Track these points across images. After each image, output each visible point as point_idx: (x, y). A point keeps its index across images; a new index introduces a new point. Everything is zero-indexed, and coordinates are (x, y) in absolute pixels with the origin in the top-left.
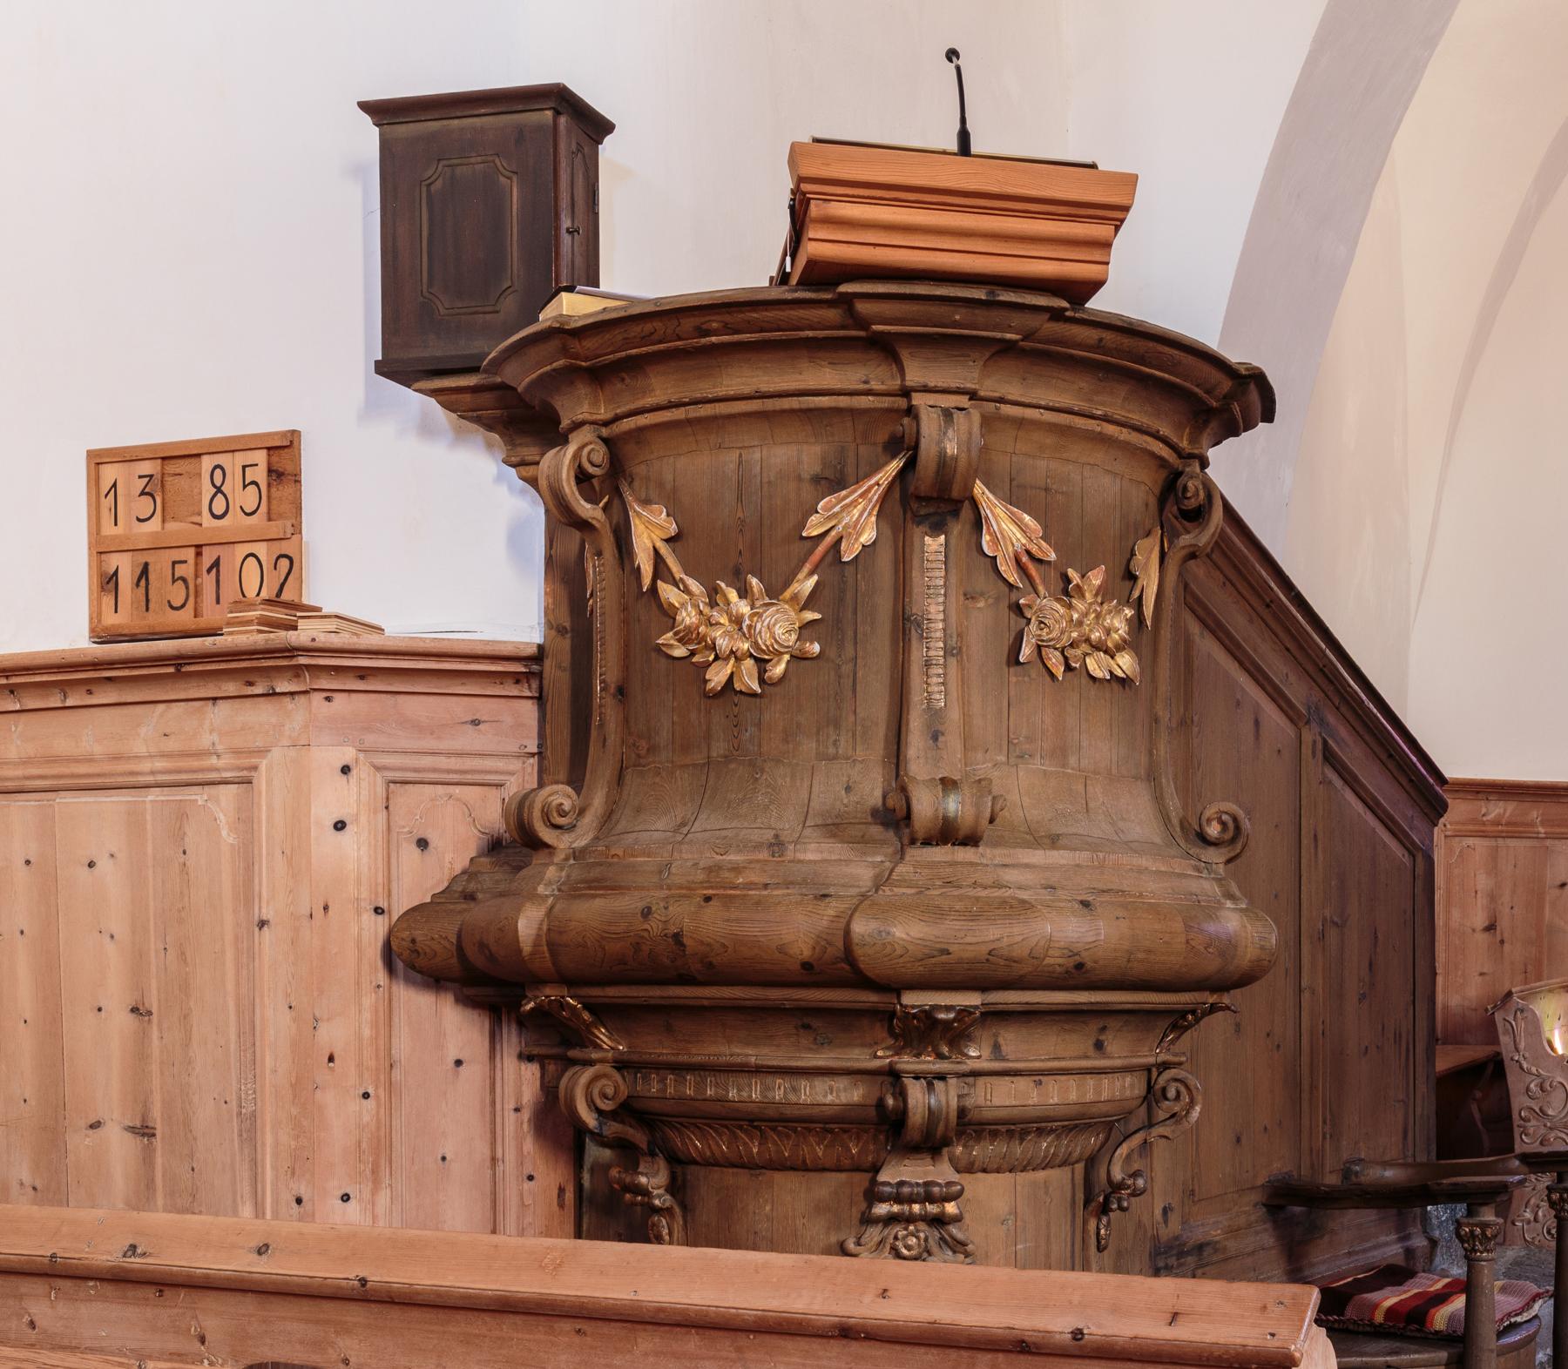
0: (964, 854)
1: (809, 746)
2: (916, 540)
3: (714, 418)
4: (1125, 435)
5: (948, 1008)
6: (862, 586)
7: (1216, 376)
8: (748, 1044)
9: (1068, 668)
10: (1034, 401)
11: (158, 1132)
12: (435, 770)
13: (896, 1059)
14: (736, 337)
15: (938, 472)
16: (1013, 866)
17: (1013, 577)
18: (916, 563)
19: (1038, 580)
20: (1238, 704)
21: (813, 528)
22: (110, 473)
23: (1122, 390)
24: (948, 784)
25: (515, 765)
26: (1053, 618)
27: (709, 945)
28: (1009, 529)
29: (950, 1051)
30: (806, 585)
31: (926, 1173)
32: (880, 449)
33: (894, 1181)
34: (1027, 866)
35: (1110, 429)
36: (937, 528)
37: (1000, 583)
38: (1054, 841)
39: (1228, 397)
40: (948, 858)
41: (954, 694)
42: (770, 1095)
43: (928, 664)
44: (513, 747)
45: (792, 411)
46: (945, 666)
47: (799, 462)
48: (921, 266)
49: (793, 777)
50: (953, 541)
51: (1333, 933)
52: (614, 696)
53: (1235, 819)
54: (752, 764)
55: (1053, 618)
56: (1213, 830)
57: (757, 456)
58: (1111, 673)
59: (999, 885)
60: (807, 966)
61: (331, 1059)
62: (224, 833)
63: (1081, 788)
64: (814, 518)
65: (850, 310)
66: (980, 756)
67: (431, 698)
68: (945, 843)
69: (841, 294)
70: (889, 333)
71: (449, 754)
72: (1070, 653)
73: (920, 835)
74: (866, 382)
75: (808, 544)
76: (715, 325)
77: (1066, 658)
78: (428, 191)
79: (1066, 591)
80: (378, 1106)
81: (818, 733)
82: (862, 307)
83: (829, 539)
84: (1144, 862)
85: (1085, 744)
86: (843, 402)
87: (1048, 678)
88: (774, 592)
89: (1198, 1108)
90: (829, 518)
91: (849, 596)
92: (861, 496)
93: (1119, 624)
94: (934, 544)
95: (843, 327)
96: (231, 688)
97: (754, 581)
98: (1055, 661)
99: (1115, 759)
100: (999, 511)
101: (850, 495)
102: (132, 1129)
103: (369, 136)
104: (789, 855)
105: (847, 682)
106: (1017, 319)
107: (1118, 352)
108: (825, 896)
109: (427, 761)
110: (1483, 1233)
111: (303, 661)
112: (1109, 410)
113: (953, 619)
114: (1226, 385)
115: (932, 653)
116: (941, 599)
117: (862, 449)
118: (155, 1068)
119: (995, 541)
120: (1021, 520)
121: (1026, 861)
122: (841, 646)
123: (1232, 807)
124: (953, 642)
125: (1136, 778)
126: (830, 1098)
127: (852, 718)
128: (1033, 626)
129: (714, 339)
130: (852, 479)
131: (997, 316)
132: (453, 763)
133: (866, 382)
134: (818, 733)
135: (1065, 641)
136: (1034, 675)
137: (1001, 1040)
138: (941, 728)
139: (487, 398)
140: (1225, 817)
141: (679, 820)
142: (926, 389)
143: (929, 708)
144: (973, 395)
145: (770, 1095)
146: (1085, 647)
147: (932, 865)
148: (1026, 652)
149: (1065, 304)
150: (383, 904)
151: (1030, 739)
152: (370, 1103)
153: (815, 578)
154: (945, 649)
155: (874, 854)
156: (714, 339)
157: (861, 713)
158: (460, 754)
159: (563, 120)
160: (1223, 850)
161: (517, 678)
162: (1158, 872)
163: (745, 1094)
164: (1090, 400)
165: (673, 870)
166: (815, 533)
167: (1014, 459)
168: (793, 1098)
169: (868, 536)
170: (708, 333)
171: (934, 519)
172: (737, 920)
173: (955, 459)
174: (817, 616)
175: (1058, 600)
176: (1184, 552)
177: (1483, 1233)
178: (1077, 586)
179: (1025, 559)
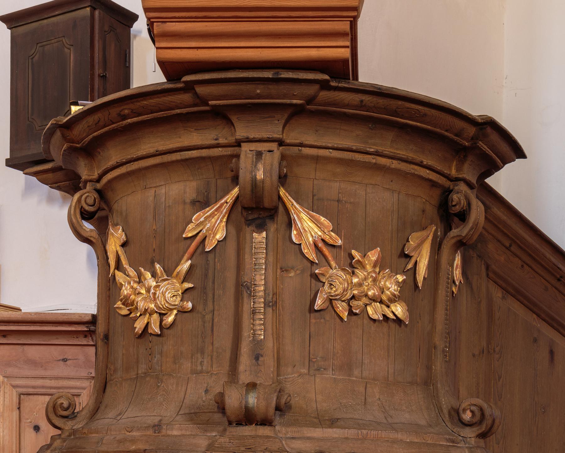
2: (248, 236)
3: (140, 170)
4: (395, 164)
6: (218, 265)
7: (459, 124)
10: (324, 144)
12: (43, 387)
15: (252, 190)
16: (299, 438)
17: (312, 255)
18: (247, 250)
20: (535, 340)
23: (390, 135)
24: (252, 386)
25: (86, 384)
26: (338, 281)
28: (309, 227)
30: (185, 266)
32: (229, 181)
34: (309, 438)
36: (261, 227)
37: (305, 261)
38: (333, 423)
39: (474, 139)
40: (253, 433)
41: (270, 331)
43: (254, 312)
45: (177, 161)
46: (265, 314)
47: (185, 192)
48: (228, 59)
50: (271, 235)
52: (102, 340)
56: (467, 416)
57: (163, 191)
58: (384, 316)
63: (362, 389)
64: (190, 226)
66: (290, 370)
67: (38, 347)
68: (251, 424)
69: (186, 82)
70: (220, 106)
71: (51, 378)
74: (216, 139)
75: (188, 242)
76: (126, 111)
77: (350, 307)
78: (32, 62)
79: (352, 266)
81: (192, 358)
82: (200, 90)
83: (198, 238)
84: (400, 436)
85: (366, 361)
86: (204, 153)
87: (338, 320)
88: (169, 272)
90: (198, 225)
92: (216, 210)
94: (260, 237)
95: (195, 105)
97: (158, 266)
98: (342, 308)
99: (391, 371)
100: (304, 216)
101: (209, 211)
104: (164, 432)
105: (208, 325)
106: (298, 89)
107: (375, 109)
109: (39, 382)
112: (380, 149)
113: (270, 285)
114: (471, 131)
115: (256, 306)
116: (263, 272)
117: (219, 181)
119: (300, 234)
121: (309, 435)
122: (205, 304)
123: (479, 402)
125: (412, 383)
128: (326, 287)
131: (284, 88)
133: (216, 139)
134: (192, 358)
135: (348, 296)
136: (328, 318)
139: (59, 175)
140: (473, 408)
141: (119, 412)
142: (249, 140)
143: (254, 340)
144: (281, 143)
146: (365, 300)
147: (244, 437)
148: (319, 303)
149: (326, 77)
153: (190, 262)
154: (265, 303)
155: (212, 431)
156: (129, 121)
157: (216, 344)
158: (57, 378)
159: (97, 13)
160: (475, 429)
161: (86, 334)
162: (411, 443)
165: (104, 442)
166: (190, 235)
167: (316, 182)
169: (219, 236)
170: (125, 117)
171: (258, 222)
173: (263, 181)
174: (191, 285)
175: (343, 270)
176: (454, 241)
178: (358, 261)
179: (320, 245)
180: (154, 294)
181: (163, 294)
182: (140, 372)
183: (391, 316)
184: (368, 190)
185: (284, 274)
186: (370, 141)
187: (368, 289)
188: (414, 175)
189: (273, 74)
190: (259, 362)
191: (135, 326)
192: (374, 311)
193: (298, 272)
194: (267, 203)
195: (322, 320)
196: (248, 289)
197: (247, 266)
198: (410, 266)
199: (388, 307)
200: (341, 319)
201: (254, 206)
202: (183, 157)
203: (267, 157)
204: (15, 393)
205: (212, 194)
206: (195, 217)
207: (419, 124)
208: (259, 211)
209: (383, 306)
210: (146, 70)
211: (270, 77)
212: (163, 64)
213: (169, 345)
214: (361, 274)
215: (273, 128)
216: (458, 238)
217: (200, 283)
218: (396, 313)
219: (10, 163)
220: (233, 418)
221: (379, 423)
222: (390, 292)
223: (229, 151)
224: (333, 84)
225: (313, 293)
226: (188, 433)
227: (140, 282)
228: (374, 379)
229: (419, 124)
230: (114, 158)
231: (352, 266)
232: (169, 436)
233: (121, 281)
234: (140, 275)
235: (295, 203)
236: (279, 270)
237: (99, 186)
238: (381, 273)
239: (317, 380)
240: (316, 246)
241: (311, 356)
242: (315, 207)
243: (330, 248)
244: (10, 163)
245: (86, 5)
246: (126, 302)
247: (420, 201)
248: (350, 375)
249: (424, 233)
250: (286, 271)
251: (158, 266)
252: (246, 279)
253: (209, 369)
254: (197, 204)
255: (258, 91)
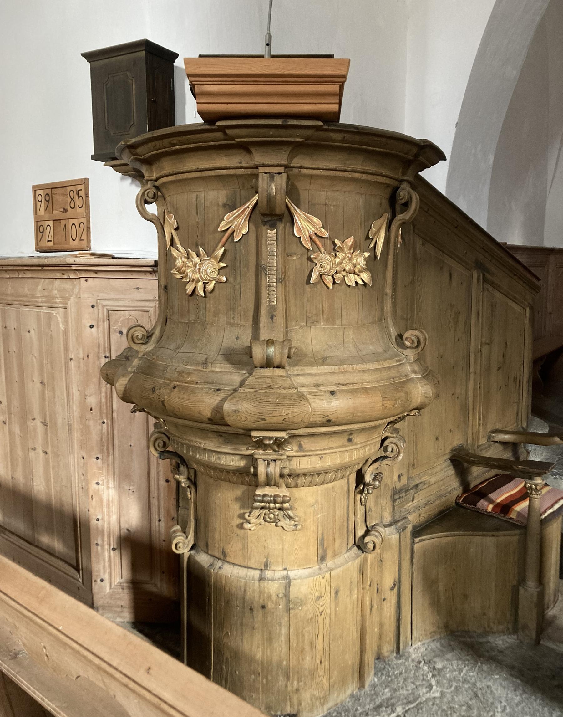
0: (279, 372)
1: (223, 319)
2: (264, 232)
4: (364, 177)
5: (270, 438)
6: (243, 252)
8: (202, 439)
9: (334, 283)
11: (48, 425)
12: (124, 306)
13: (256, 451)
14: (185, 146)
17: (308, 246)
18: (264, 242)
19: (320, 245)
21: (223, 226)
22: (38, 192)
24: (270, 342)
25: (153, 304)
26: (325, 262)
27: (174, 407)
28: (306, 225)
29: (279, 449)
31: (276, 491)
33: (261, 494)
35: (356, 175)
36: (273, 227)
37: (303, 248)
40: (271, 374)
42: (210, 458)
44: (152, 298)
47: (218, 198)
49: (217, 332)
50: (280, 232)
51: (485, 349)
53: (418, 338)
54: (203, 325)
55: (325, 262)
57: (203, 195)
59: (293, 387)
60: (209, 419)
61: (91, 410)
62: (61, 325)
63: (341, 333)
64: (223, 223)
65: (225, 133)
66: (294, 323)
68: (270, 368)
70: (243, 142)
71: (129, 300)
72: (336, 276)
73: (258, 365)
77: (334, 279)
79: (335, 249)
80: (108, 426)
83: (229, 232)
86: (232, 172)
89: (402, 455)
91: (238, 256)
93: (360, 260)
94: (272, 233)
96: (58, 275)
97: (201, 249)
98: (329, 280)
99: (360, 318)
101: (236, 212)
102: (42, 422)
103: (86, 66)
104: (209, 369)
106: (299, 132)
108: (218, 390)
109: (121, 303)
110: (536, 488)
111: (74, 268)
112: (355, 167)
113: (280, 266)
116: (275, 257)
118: (47, 403)
119: (299, 231)
120: (312, 220)
121: (309, 372)
122: (235, 278)
124: (280, 276)
126: (232, 463)
127: (239, 308)
128: (318, 265)
129: (177, 147)
130: (238, 205)
131: (289, 132)
132: (130, 304)
133: (240, 163)
135: (333, 272)
137: (302, 443)
138: (275, 314)
142: (264, 166)
143: (270, 305)
145: (210, 458)
146: (344, 273)
147: (264, 377)
149: (320, 123)
150: (108, 355)
151: (317, 315)
152: (105, 425)
153: (223, 249)
154: (276, 279)
155: (243, 369)
157: (243, 306)
161: (151, 273)
163: (202, 457)
164: (345, 164)
167: (310, 192)
168: (218, 461)
169: (244, 231)
171: (272, 222)
172: (183, 399)
173: (275, 197)
174: (225, 265)
176: (399, 222)
177: (536, 488)
178: (339, 247)
179: (314, 237)
180: (199, 269)
181: (206, 270)
182: (191, 319)
183: (360, 282)
184: (346, 195)
185: (290, 258)
186: (348, 162)
187: (346, 266)
188: (376, 182)
189: (283, 122)
190: (274, 321)
191: (186, 288)
192: (351, 280)
193: (299, 256)
194: (278, 211)
195: (315, 289)
196: (265, 269)
197: (264, 254)
198: (372, 245)
199: (358, 275)
200: (328, 287)
201: (269, 213)
202: (217, 174)
203: (277, 177)
204: (105, 310)
205: (238, 200)
206: (226, 216)
207: (382, 150)
208: (272, 215)
209: (356, 276)
210: (189, 114)
211: (281, 123)
212: (201, 113)
213: (210, 304)
214: (340, 255)
215: (281, 157)
216: (403, 221)
217: (232, 261)
218: (364, 279)
219: (94, 158)
220: (258, 365)
221: (353, 357)
222: (361, 266)
223: (249, 171)
224: (325, 127)
225: (309, 270)
226: (226, 370)
227: (188, 258)
228: (349, 325)
229: (382, 150)
230: (167, 169)
231: (335, 249)
232: (213, 372)
233: (175, 255)
234: (188, 253)
235: (296, 208)
236: (286, 256)
237: (157, 184)
238: (354, 254)
239: (312, 330)
240: (311, 238)
241: (308, 314)
242: (310, 210)
243: (320, 239)
244: (94, 158)
245: (142, 49)
246: (179, 271)
247: (379, 198)
248: (333, 325)
249: (381, 220)
250: (291, 255)
251: (201, 249)
252: (263, 263)
253: (239, 322)
254: (227, 206)
255: (271, 133)
